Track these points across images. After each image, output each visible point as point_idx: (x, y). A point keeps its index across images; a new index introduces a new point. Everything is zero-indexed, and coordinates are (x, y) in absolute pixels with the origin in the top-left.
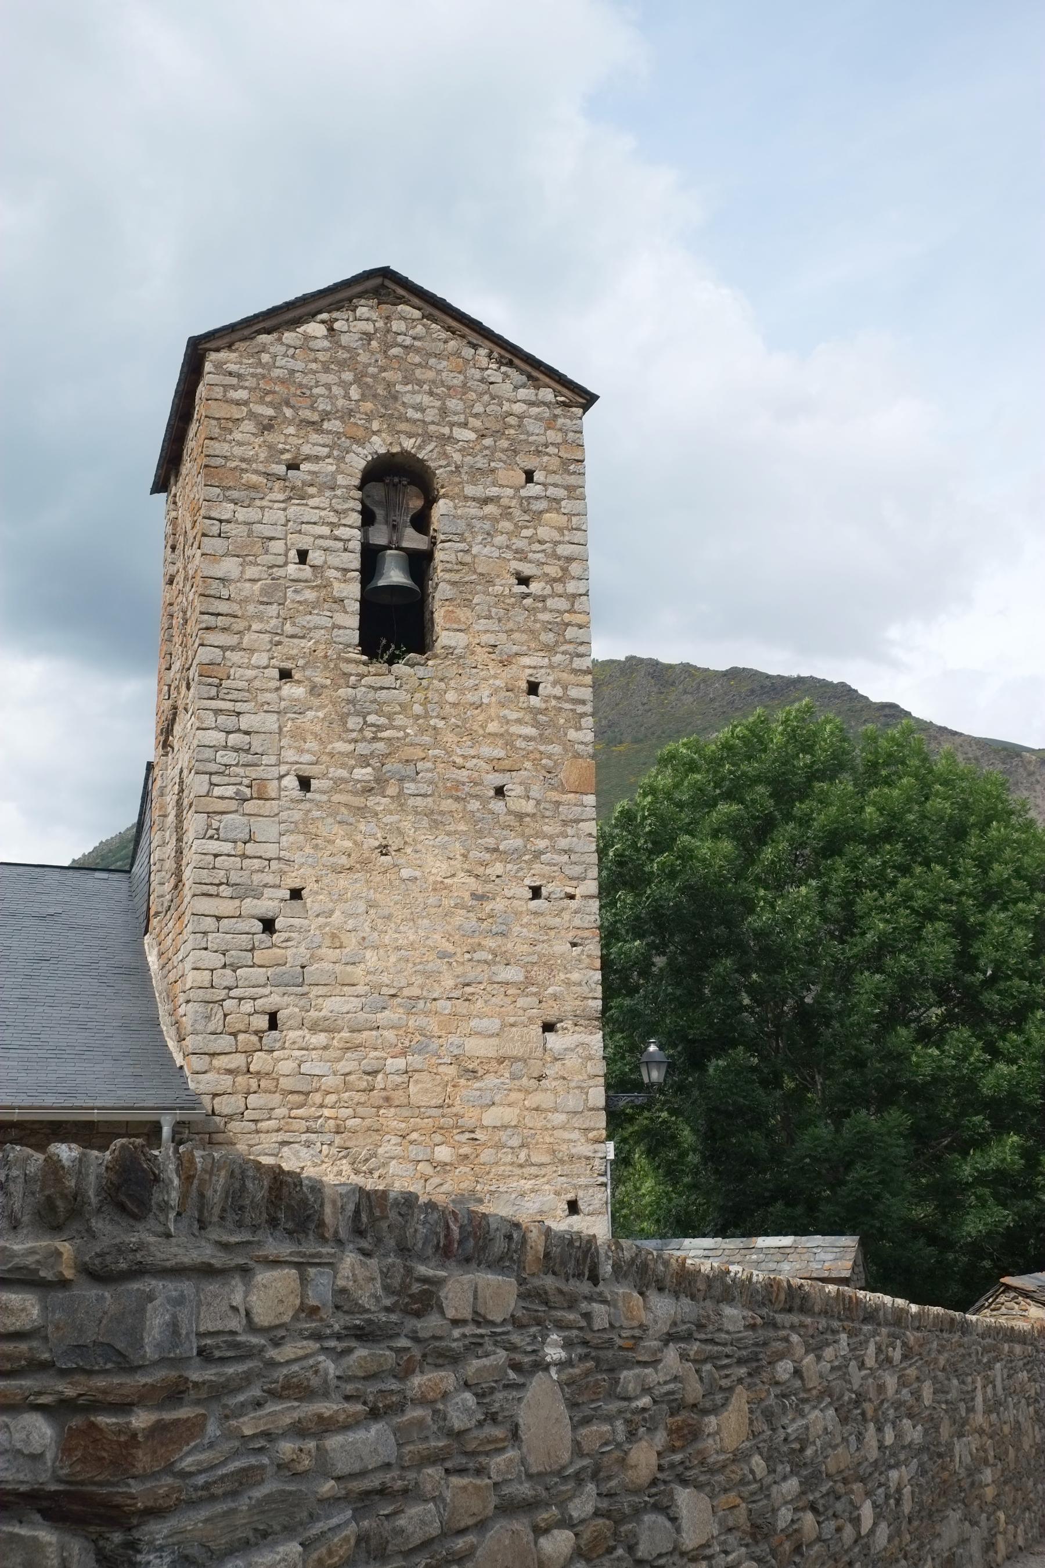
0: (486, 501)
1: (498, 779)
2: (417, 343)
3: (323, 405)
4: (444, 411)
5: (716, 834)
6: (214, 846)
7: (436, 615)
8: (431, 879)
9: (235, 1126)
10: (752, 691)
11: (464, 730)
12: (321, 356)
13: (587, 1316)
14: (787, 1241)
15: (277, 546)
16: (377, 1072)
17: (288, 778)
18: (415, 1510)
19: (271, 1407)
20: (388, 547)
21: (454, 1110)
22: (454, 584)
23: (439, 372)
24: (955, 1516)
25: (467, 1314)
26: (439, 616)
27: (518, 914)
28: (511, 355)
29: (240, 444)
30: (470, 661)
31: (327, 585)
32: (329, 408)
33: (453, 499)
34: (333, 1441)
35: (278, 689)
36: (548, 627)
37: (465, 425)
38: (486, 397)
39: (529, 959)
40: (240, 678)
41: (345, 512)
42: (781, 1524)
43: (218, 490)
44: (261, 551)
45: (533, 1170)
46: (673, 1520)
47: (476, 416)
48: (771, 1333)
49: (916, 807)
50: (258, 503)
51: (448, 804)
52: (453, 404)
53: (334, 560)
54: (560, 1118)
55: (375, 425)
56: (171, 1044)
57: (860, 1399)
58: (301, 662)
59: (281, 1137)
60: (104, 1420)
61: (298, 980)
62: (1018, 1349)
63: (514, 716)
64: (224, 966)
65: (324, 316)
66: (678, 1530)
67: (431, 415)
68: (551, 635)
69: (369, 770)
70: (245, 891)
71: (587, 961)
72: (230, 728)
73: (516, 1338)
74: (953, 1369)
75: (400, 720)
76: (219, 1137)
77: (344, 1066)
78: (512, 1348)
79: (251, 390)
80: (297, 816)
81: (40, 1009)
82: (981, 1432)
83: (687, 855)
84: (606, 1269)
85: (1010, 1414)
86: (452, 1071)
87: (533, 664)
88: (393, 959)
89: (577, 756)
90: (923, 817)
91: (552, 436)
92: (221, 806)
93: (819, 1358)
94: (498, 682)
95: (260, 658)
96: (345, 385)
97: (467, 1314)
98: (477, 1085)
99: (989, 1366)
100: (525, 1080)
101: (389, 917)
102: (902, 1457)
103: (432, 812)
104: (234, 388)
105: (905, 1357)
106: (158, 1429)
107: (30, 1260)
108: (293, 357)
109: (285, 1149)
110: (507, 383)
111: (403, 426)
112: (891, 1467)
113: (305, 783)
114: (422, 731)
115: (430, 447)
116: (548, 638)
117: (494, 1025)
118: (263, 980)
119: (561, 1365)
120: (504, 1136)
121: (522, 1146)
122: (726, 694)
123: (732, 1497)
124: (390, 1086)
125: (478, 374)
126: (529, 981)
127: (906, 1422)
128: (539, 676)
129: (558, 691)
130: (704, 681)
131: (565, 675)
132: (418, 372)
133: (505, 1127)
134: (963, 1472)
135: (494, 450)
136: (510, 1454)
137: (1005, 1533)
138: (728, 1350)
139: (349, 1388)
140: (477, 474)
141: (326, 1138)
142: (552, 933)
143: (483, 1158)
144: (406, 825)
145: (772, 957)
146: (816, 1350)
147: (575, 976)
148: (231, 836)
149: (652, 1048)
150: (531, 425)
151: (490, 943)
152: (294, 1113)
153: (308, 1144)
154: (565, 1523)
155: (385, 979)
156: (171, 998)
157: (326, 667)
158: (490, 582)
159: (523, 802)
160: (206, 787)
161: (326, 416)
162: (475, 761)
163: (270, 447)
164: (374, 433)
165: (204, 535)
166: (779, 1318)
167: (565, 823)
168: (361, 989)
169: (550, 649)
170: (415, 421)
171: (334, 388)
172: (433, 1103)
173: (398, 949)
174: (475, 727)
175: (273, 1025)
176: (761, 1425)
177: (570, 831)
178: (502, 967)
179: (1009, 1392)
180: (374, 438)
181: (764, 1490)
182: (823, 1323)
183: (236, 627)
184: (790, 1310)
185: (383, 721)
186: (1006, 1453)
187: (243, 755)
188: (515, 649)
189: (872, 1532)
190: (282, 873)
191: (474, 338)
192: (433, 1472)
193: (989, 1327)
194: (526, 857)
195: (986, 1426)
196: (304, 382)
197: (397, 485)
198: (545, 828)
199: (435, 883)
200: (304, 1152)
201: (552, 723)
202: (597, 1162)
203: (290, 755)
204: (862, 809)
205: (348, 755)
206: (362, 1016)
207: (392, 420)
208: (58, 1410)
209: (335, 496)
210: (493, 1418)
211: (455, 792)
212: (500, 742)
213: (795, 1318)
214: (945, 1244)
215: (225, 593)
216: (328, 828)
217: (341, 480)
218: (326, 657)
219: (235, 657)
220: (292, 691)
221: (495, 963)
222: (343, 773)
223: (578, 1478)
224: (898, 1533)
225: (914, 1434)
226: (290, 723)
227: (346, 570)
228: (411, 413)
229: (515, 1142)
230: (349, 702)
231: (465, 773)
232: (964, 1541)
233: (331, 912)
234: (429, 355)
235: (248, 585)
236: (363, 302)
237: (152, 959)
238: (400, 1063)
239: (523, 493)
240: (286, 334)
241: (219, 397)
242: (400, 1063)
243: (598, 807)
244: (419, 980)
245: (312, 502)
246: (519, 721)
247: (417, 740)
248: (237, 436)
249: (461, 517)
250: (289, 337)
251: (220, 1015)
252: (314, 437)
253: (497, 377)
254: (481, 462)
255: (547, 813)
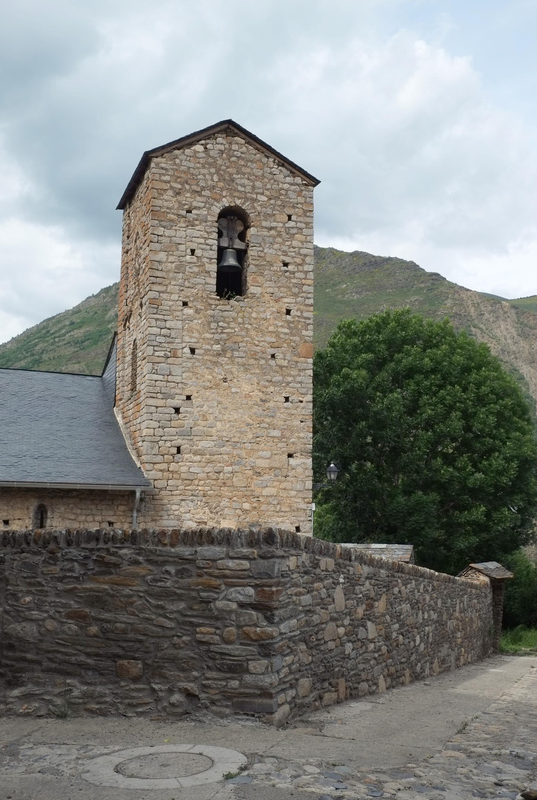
0: (271, 229)
1: (271, 351)
2: (243, 155)
3: (202, 184)
4: (254, 187)
5: (359, 367)
6: (155, 377)
7: (248, 278)
8: (244, 393)
9: (163, 493)
10: (365, 264)
11: (258, 330)
12: (201, 161)
13: (348, 571)
14: (384, 546)
15: (182, 247)
16: (220, 472)
17: (186, 349)
18: (315, 616)
19: (292, 589)
20: (228, 248)
21: (251, 488)
22: (256, 265)
23: (252, 169)
24: (446, 646)
25: (324, 569)
26: (249, 279)
27: (279, 408)
28: (284, 162)
29: (166, 201)
30: (262, 300)
31: (203, 265)
32: (204, 185)
33: (257, 227)
34: (302, 598)
35: (182, 310)
36: (295, 285)
37: (263, 194)
38: (272, 181)
39: (283, 427)
40: (166, 305)
41: (211, 232)
42: (393, 637)
43: (157, 222)
44: (175, 249)
45: (282, 514)
46: (367, 630)
47: (268, 190)
48: (393, 579)
49: (448, 359)
50: (174, 228)
51: (252, 361)
52: (258, 184)
53: (206, 254)
54: (293, 493)
55: (224, 193)
56: (134, 458)
57: (418, 602)
58: (192, 299)
59: (181, 497)
60: (265, 589)
61: (188, 434)
62: (474, 591)
63: (280, 324)
64: (159, 427)
65: (203, 142)
66: (368, 633)
67: (248, 189)
68: (297, 289)
69: (219, 346)
70: (167, 396)
71: (307, 428)
72: (162, 327)
73: (334, 575)
74: (449, 596)
75: (232, 325)
76: (157, 497)
77: (207, 469)
78: (333, 578)
79: (171, 176)
80: (190, 365)
81: (77, 441)
82: (458, 619)
83: (346, 377)
84: (353, 558)
85: (469, 614)
86: (251, 472)
87: (289, 301)
88: (228, 426)
89: (306, 342)
90: (451, 363)
91: (300, 200)
92: (158, 360)
93: (406, 588)
94: (274, 309)
95: (175, 297)
96: (212, 175)
97: (324, 569)
98: (261, 478)
99: (462, 596)
100: (280, 477)
101: (226, 408)
102: (430, 623)
103: (245, 365)
104: (164, 175)
105: (433, 590)
106: (277, 591)
107: (247, 554)
108: (189, 161)
109: (183, 502)
110: (281, 173)
111: (236, 194)
112: (426, 626)
113: (193, 351)
114: (242, 330)
115: (247, 204)
116: (296, 290)
117: (268, 454)
118: (175, 433)
119: (343, 583)
120: (270, 500)
121: (278, 504)
122: (351, 264)
123: (381, 626)
124: (225, 478)
125: (269, 170)
126: (283, 436)
127: (432, 612)
128: (291, 307)
129: (299, 314)
130: (340, 257)
131: (302, 307)
132: (243, 168)
133: (271, 496)
134: (450, 632)
135: (275, 205)
136: (333, 605)
137: (464, 656)
138: (381, 583)
139: (304, 585)
140: (268, 216)
141: (199, 498)
142: (293, 417)
143: (262, 508)
144: (234, 370)
145: (380, 424)
146: (405, 585)
147: (302, 435)
148: (162, 373)
149: (332, 465)
150: (291, 194)
151: (268, 420)
152: (187, 488)
153: (192, 501)
154: (343, 626)
155: (224, 434)
156: (132, 437)
157: (202, 301)
158: (272, 265)
159: (283, 361)
160: (152, 351)
161: (203, 189)
162: (263, 343)
163: (180, 203)
164: (224, 197)
165: (151, 242)
166: (396, 574)
167: (300, 370)
168: (215, 438)
169: (296, 295)
170: (242, 192)
171: (207, 176)
172: (243, 485)
173: (230, 421)
174: (264, 329)
175: (179, 452)
176: (389, 607)
177: (302, 374)
178: (272, 430)
179: (469, 606)
180: (224, 199)
181: (389, 626)
182: (408, 577)
183: (164, 283)
184: (398, 572)
185: (225, 325)
186: (466, 628)
187: (167, 338)
188: (281, 295)
189: (419, 645)
190: (183, 389)
191: (268, 153)
192: (318, 608)
193: (463, 582)
194: (283, 385)
195: (459, 617)
196: (194, 172)
197: (233, 220)
198: (292, 372)
199: (246, 394)
200: (190, 504)
201: (296, 328)
202: (308, 511)
203: (187, 339)
204: (422, 359)
205: (211, 339)
206: (215, 449)
207: (232, 191)
208: (255, 587)
209: (207, 225)
210: (329, 596)
211: (254, 356)
212: (274, 335)
213: (399, 574)
214: (448, 548)
215: (160, 268)
216: (203, 370)
217: (209, 218)
218: (202, 297)
219: (164, 296)
220: (188, 311)
221: (269, 429)
222: (209, 347)
223: (346, 614)
224: (427, 647)
225: (434, 616)
226: (187, 325)
227: (211, 259)
228: (240, 188)
229: (275, 502)
230: (211, 316)
231: (259, 348)
232: (449, 655)
233: (203, 406)
234: (248, 161)
235: (170, 264)
236: (220, 135)
237: (119, 419)
238: (230, 469)
239: (287, 225)
240: (187, 150)
241: (158, 179)
242: (230, 469)
243: (314, 364)
244: (238, 435)
245: (197, 228)
246: (282, 326)
247: (239, 334)
248: (166, 197)
249: (260, 236)
250: (187, 151)
251: (157, 447)
252: (198, 198)
253: (276, 172)
254: (269, 211)
255: (293, 366)
